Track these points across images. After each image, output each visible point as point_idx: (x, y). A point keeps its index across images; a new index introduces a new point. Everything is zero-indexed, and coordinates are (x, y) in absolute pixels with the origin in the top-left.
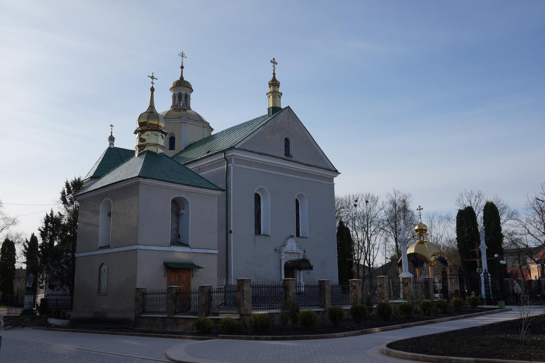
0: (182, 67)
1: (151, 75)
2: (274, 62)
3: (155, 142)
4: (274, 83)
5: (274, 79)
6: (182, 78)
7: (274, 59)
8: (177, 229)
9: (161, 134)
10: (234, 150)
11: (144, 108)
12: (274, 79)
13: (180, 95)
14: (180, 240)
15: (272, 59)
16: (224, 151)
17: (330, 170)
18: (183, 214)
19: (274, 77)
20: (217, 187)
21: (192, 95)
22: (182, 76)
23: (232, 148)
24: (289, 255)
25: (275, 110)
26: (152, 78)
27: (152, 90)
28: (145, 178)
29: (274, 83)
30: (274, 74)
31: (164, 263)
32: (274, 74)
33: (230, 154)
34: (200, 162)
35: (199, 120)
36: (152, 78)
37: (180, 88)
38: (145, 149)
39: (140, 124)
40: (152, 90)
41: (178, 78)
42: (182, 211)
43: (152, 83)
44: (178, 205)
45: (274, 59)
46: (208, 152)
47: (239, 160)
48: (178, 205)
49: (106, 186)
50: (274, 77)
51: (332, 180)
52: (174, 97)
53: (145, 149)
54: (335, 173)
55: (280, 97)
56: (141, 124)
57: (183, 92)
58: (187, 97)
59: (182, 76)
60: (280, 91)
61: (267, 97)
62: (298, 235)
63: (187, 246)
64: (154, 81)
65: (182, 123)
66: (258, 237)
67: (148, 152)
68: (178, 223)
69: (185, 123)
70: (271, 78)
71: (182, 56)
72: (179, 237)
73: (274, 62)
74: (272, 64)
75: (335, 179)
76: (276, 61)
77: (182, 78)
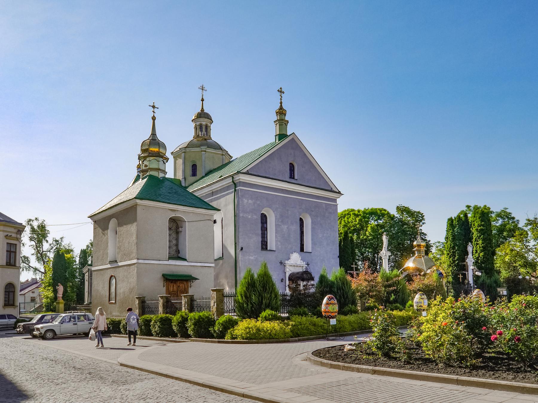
0: (203, 100)
1: (152, 104)
2: (281, 91)
3: (156, 167)
4: (281, 112)
5: (281, 108)
6: (202, 110)
7: (281, 88)
8: (177, 245)
9: (162, 159)
10: (240, 175)
11: (147, 135)
12: (281, 108)
13: (201, 126)
14: (179, 255)
15: (279, 88)
16: (232, 176)
17: (332, 191)
18: (181, 232)
19: (281, 105)
20: (213, 207)
21: (212, 126)
22: (202, 108)
23: (239, 172)
24: (293, 268)
25: (282, 136)
26: (154, 107)
27: (154, 118)
28: (141, 199)
29: (281, 112)
30: (281, 103)
31: (164, 275)
32: (281, 103)
33: (237, 178)
34: (212, 186)
35: (218, 147)
36: (154, 107)
37: (201, 119)
38: (148, 174)
39: (142, 150)
40: (154, 118)
41: (199, 110)
42: (180, 229)
43: (154, 112)
44: (176, 226)
45: (281, 88)
46: (220, 177)
47: (245, 184)
48: (176, 226)
49: (113, 206)
50: (281, 105)
51: (335, 201)
52: (196, 128)
53: (148, 174)
54: (339, 195)
55: (286, 125)
56: (143, 151)
57: (204, 123)
58: (207, 128)
59: (202, 108)
60: (286, 119)
61: (274, 124)
62: (302, 250)
63: (185, 260)
64: (156, 110)
65: (202, 151)
66: (264, 252)
67: (150, 176)
68: (177, 239)
69: (205, 151)
70: (278, 106)
71: (202, 89)
72: (178, 252)
73: (281, 91)
74: (279, 94)
75: (338, 200)
76: (283, 90)
77: (202, 110)
